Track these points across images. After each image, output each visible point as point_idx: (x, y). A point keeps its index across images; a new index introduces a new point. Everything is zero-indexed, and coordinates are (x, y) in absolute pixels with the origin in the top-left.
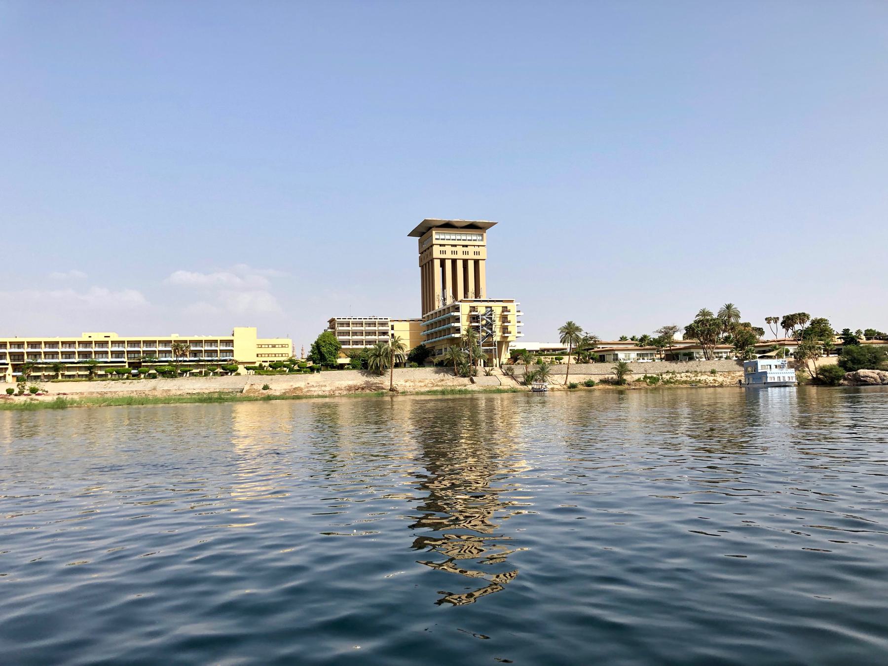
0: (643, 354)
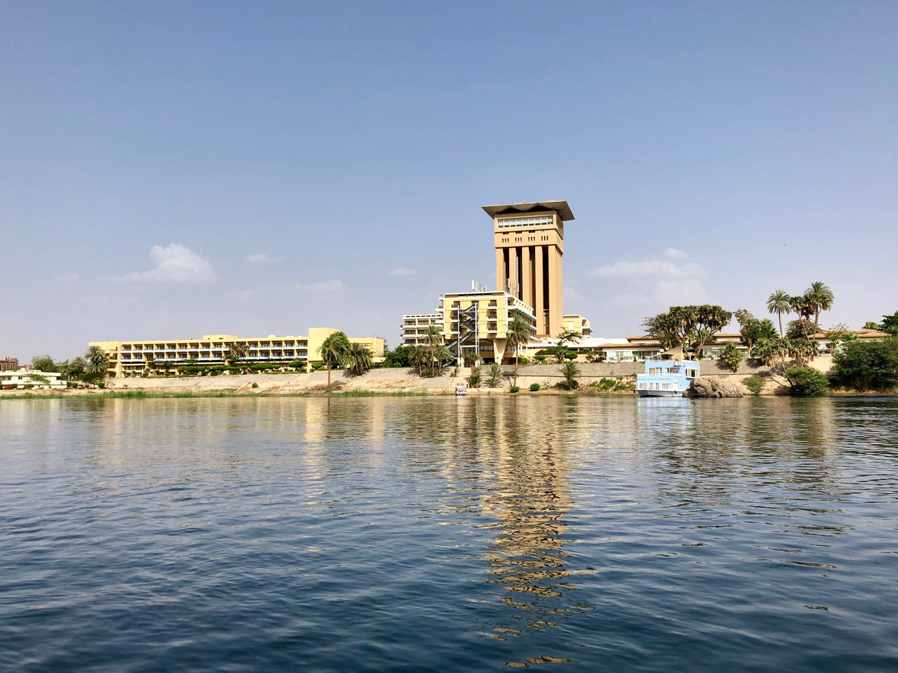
0: (643, 352)
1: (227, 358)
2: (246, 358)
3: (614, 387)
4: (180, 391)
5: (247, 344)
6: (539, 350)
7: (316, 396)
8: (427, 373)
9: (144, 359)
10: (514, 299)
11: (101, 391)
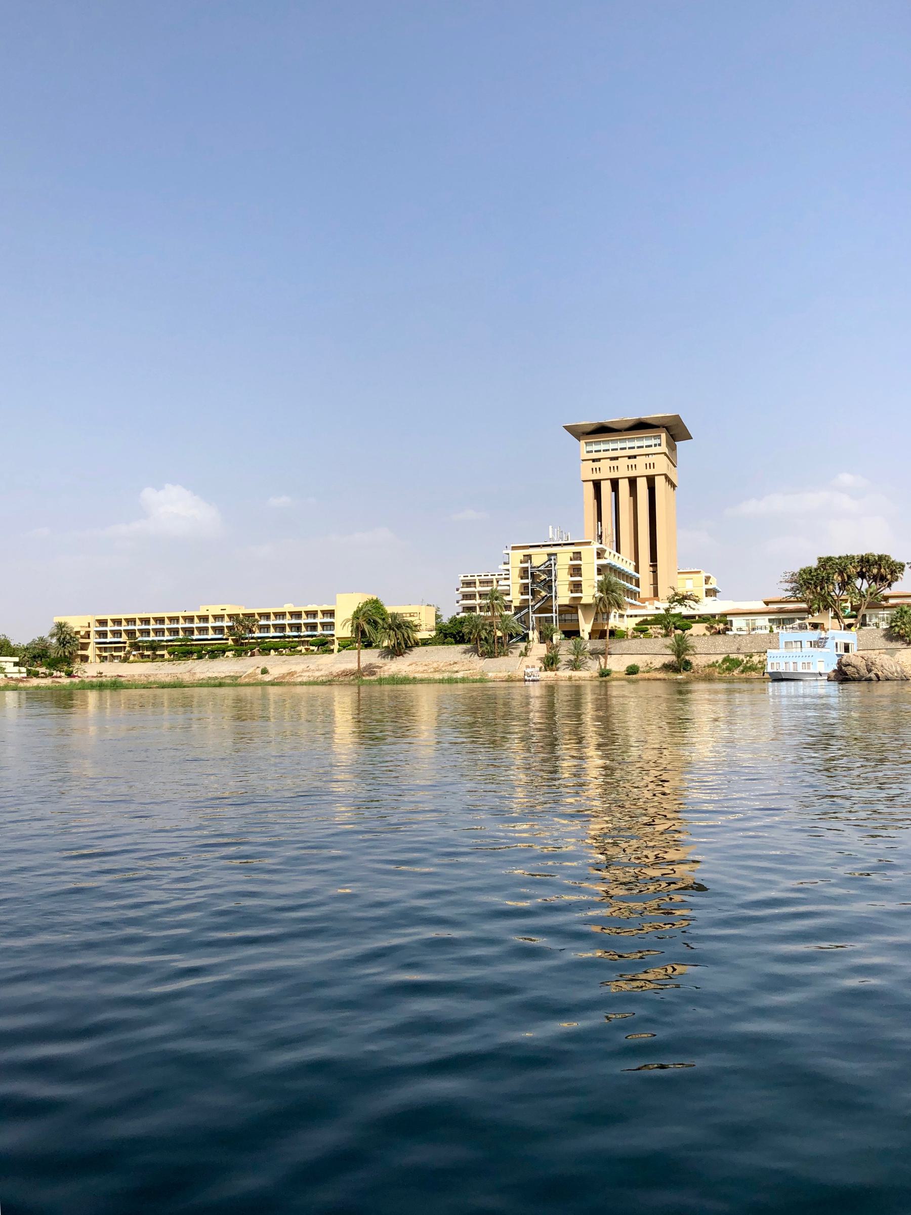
0: (783, 619)
1: (231, 635)
2: (255, 635)
3: (741, 668)
4: (168, 679)
5: (257, 617)
6: (641, 619)
7: (341, 684)
8: (488, 652)
9: (124, 638)
10: (605, 550)
11: (66, 681)
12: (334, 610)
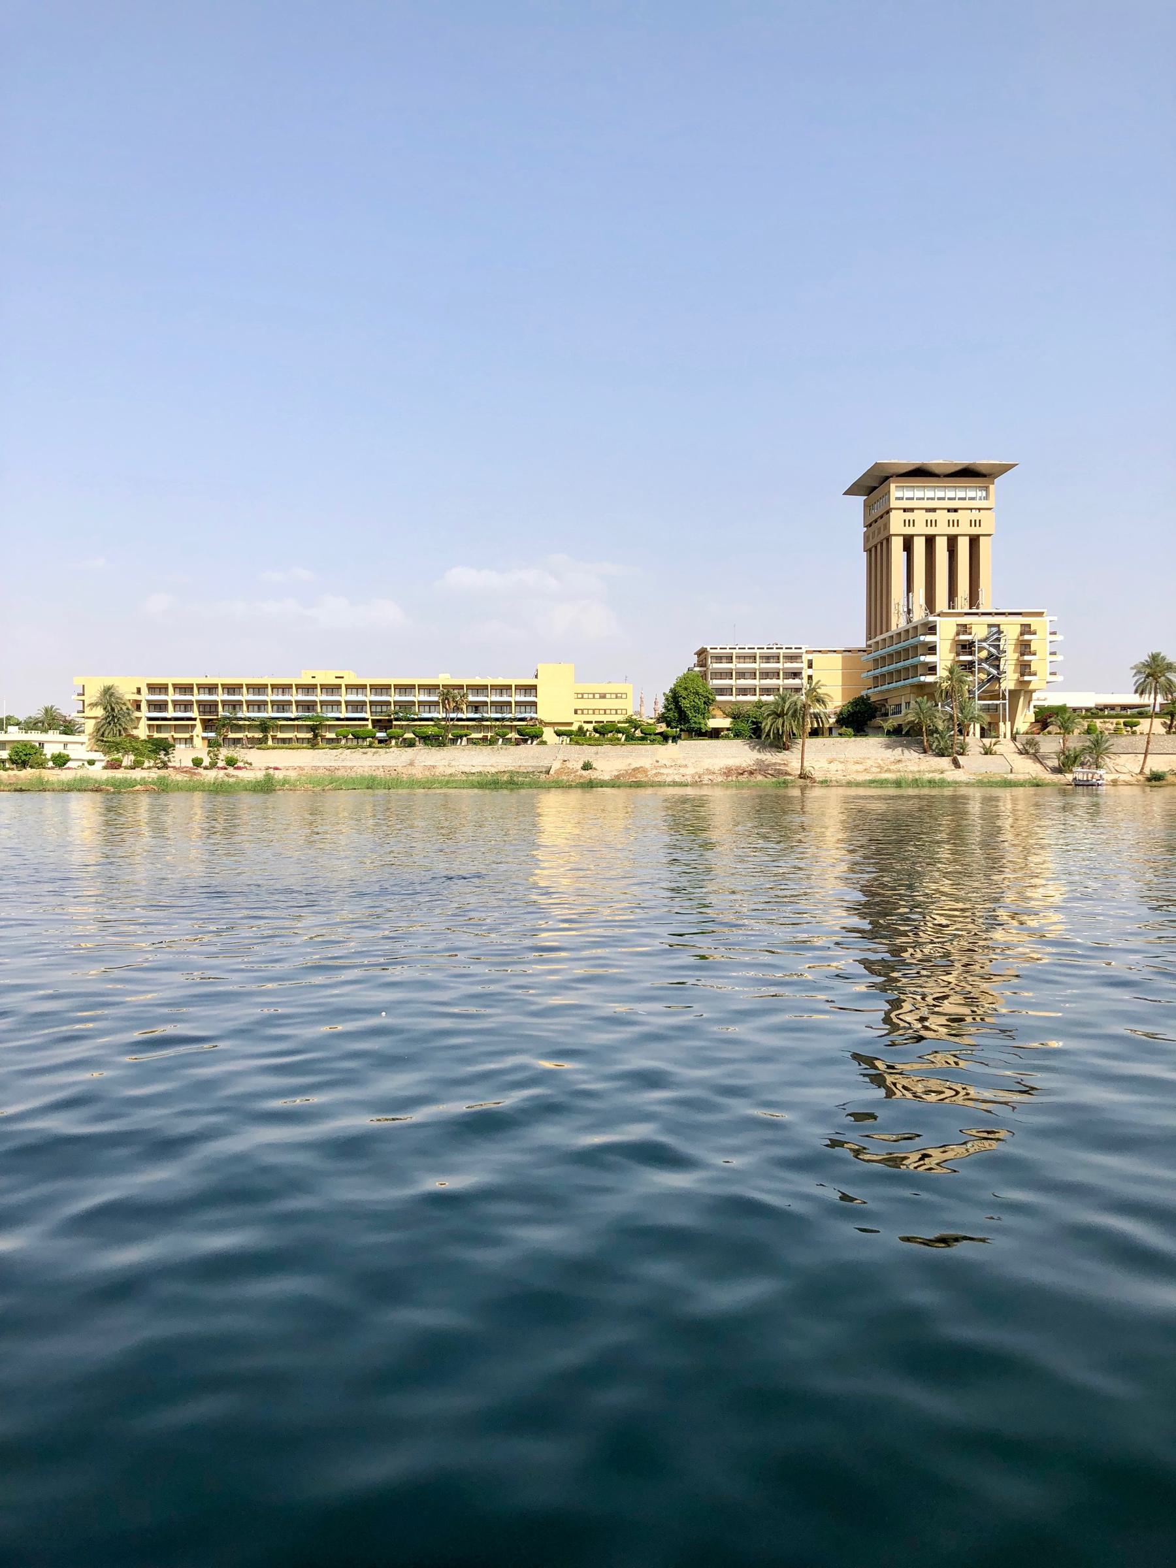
9: (195, 713)
12: (536, 686)
